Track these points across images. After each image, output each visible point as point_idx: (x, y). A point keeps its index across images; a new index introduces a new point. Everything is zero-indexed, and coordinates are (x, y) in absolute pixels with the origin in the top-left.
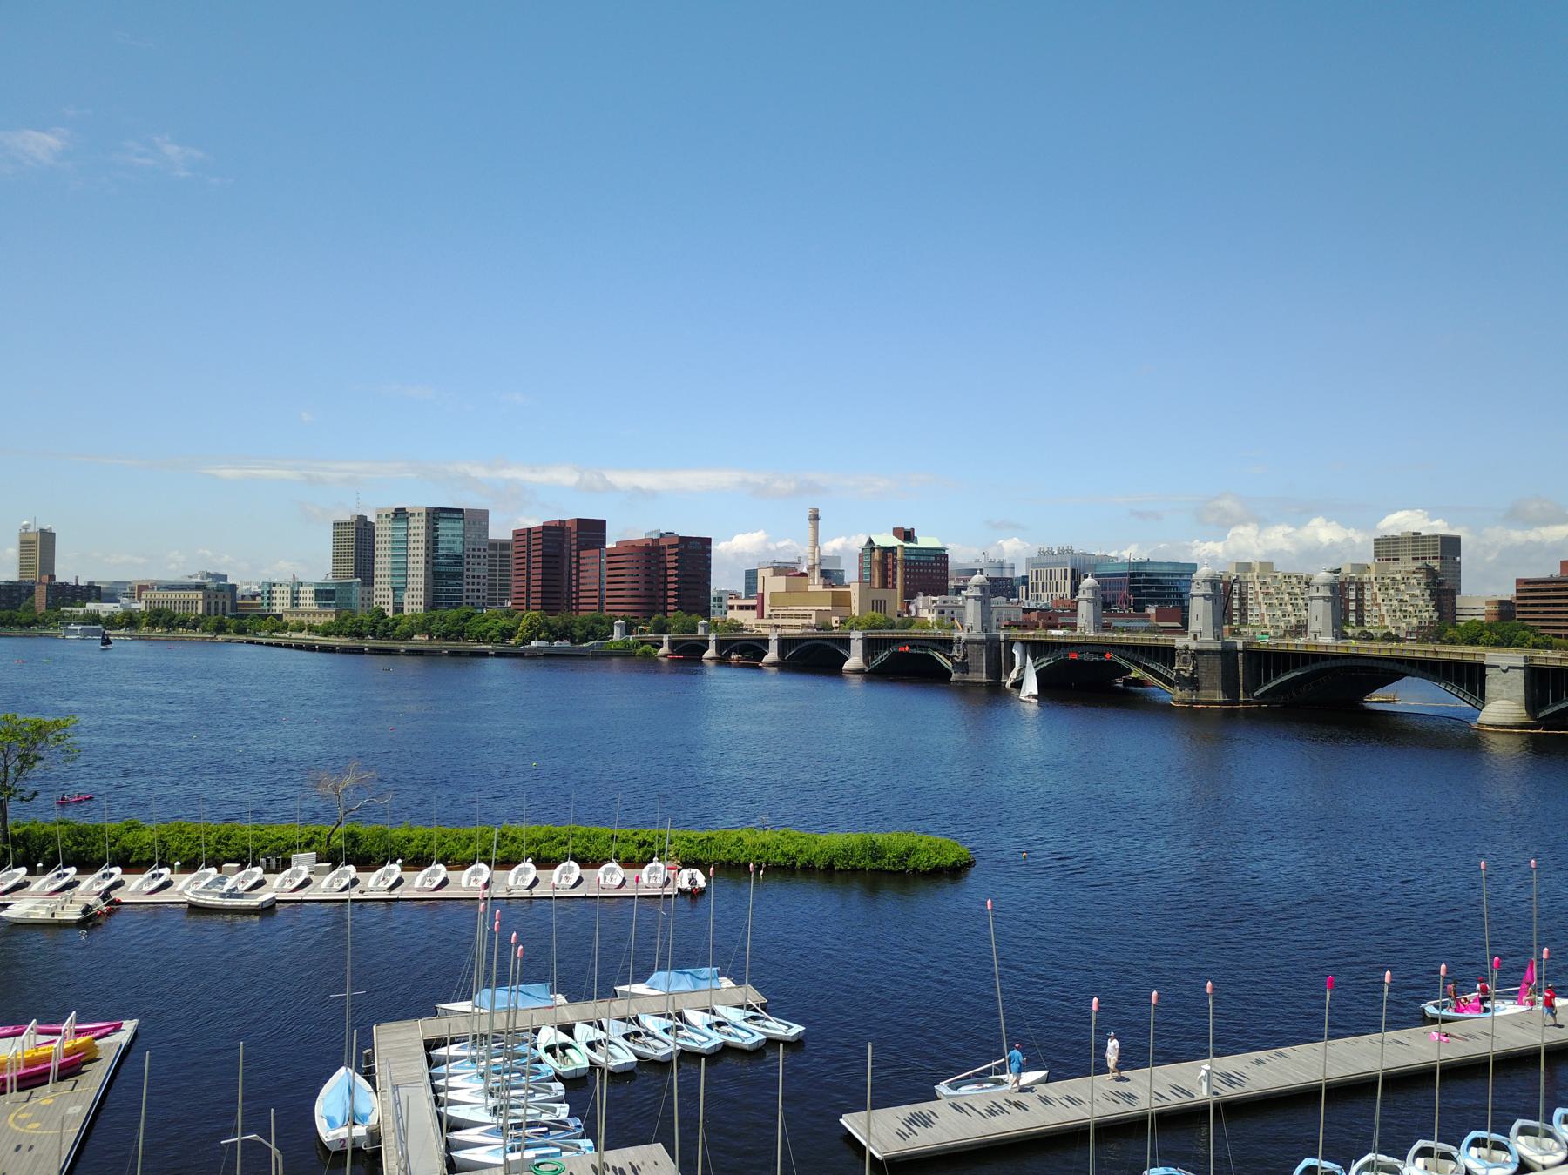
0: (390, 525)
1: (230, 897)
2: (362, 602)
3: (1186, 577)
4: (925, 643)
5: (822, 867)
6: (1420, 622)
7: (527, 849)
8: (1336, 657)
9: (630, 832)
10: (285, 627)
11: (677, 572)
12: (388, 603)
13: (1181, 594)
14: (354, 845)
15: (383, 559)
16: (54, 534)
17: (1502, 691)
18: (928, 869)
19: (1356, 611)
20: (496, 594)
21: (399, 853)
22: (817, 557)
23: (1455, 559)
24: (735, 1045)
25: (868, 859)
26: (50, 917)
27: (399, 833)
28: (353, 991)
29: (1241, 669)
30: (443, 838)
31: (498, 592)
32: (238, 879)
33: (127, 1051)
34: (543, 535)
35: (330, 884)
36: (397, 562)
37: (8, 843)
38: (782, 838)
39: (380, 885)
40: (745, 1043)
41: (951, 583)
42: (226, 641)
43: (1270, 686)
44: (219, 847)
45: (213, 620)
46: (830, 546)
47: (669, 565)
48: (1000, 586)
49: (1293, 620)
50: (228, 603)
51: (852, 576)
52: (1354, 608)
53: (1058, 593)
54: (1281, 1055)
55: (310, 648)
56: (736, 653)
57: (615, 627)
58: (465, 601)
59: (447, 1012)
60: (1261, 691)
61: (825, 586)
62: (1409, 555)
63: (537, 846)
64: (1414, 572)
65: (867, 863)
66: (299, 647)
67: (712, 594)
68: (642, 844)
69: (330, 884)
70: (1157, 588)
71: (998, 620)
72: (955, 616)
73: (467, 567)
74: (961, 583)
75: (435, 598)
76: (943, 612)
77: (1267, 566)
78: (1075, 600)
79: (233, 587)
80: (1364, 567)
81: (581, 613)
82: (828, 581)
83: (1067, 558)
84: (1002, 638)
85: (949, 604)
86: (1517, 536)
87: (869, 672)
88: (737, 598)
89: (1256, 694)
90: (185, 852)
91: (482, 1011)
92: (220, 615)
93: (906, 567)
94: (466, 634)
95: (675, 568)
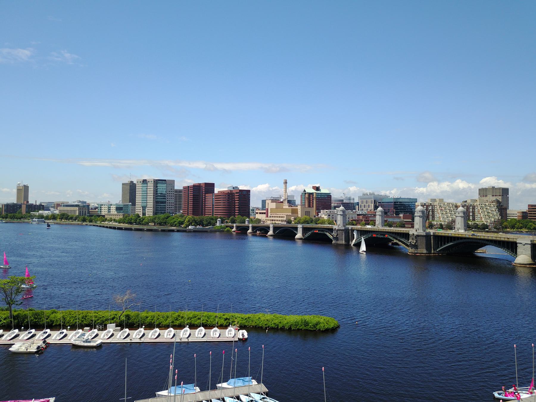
0: (141, 185)
1: (86, 342)
2: (132, 211)
3: (413, 203)
5: (287, 329)
6: (495, 220)
7: (187, 321)
8: (465, 238)
9: (222, 314)
10: (106, 220)
11: (238, 202)
12: (140, 212)
14: (128, 319)
15: (139, 197)
16: (28, 186)
17: (523, 252)
18: (324, 330)
19: (472, 216)
20: (177, 208)
21: (143, 322)
22: (286, 196)
23: (507, 196)
25: (303, 326)
26: (26, 351)
29: (432, 242)
31: (178, 207)
34: (193, 192)
36: (144, 198)
37: (12, 318)
38: (273, 317)
41: (333, 205)
43: (442, 248)
44: (83, 320)
45: (81, 217)
46: (291, 189)
47: (236, 199)
48: (349, 206)
49: (450, 219)
50: (87, 211)
51: (298, 201)
52: (471, 211)
55: (114, 228)
56: (259, 231)
58: (167, 211)
59: (159, 395)
61: (289, 206)
65: (303, 327)
66: (110, 228)
67: (250, 208)
68: (226, 319)
70: (403, 207)
71: (348, 218)
72: (334, 217)
75: (156, 210)
76: (330, 215)
78: (375, 211)
80: (475, 201)
82: (290, 205)
83: (372, 196)
84: (350, 229)
85: (332, 213)
86: (528, 186)
87: (304, 239)
88: (259, 210)
89: (437, 250)
93: (317, 200)
94: (167, 223)
95: (238, 200)
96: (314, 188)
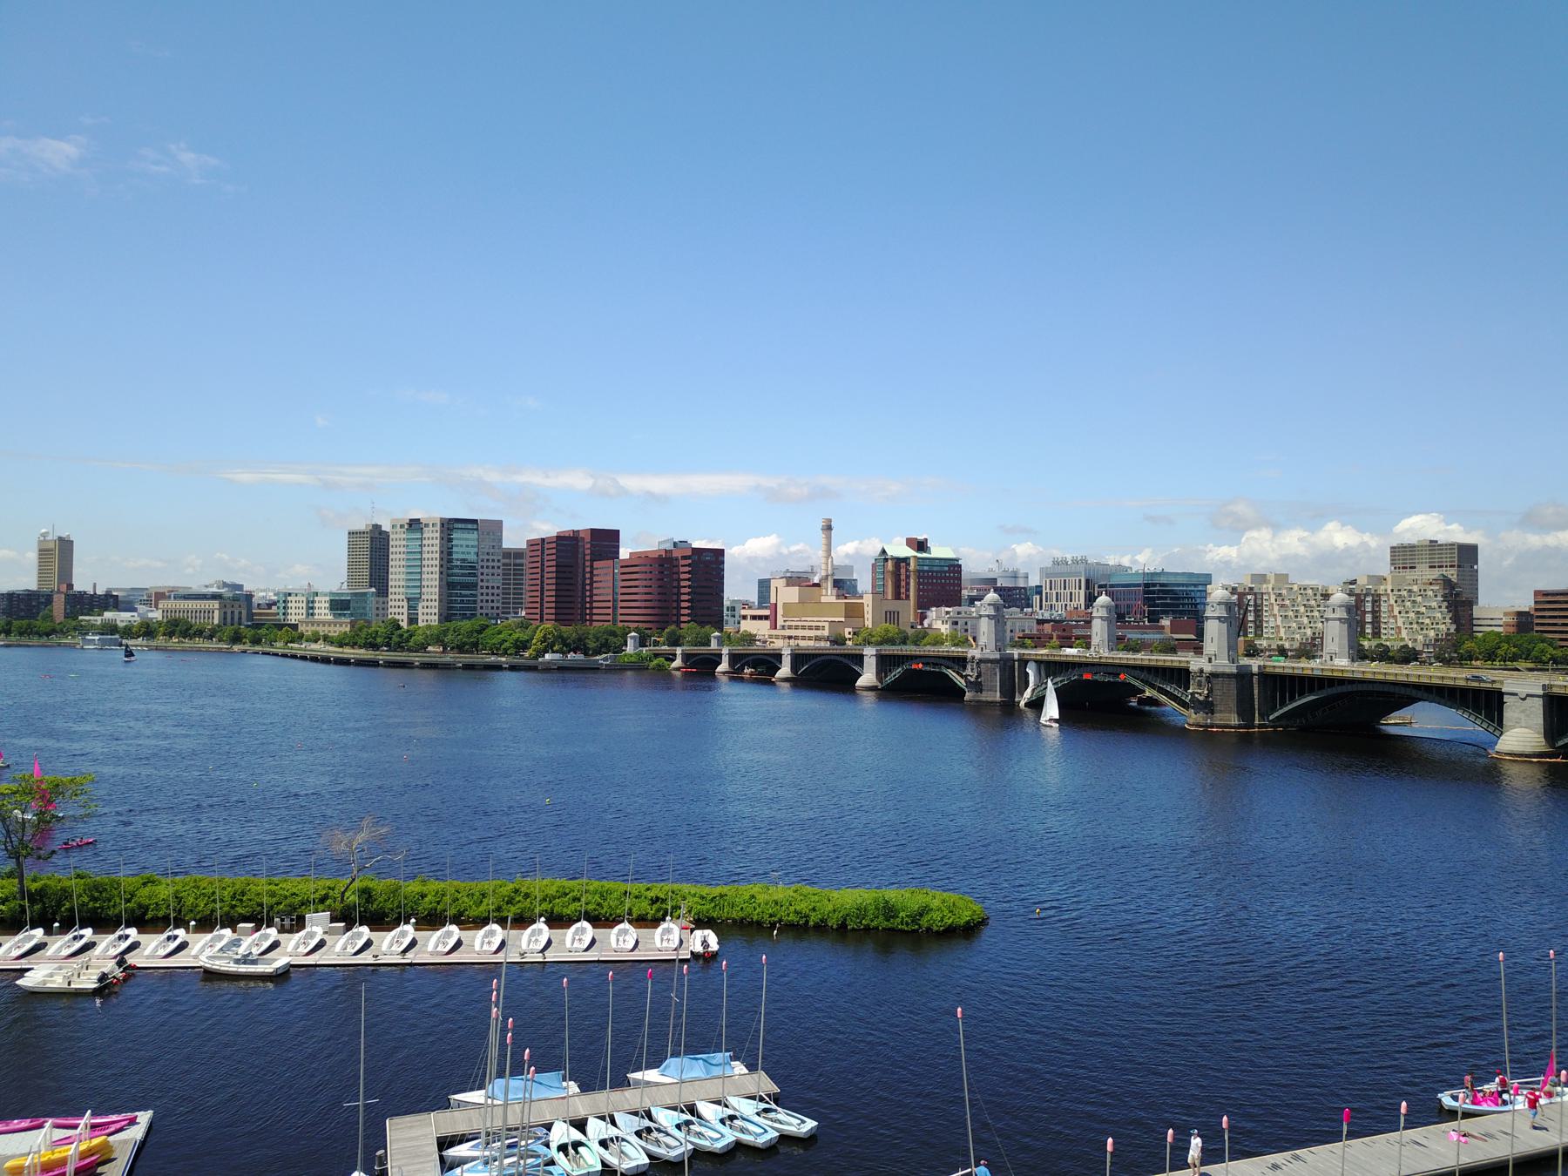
0: (404, 536)
1: (245, 963)
3: (1200, 588)
4: (942, 661)
5: (835, 927)
6: (1437, 635)
7: (540, 905)
8: (1352, 681)
11: (690, 583)
12: (403, 614)
13: (1196, 605)
15: (398, 570)
16: (72, 541)
17: (1520, 719)
18: (941, 928)
19: (1372, 623)
20: (511, 601)
21: (412, 909)
23: (1472, 567)
24: (745, 1143)
25: (881, 918)
26: (66, 986)
27: (413, 887)
28: (369, 1098)
29: (1256, 692)
30: (457, 894)
32: (252, 941)
33: (142, 1146)
35: (343, 947)
38: (794, 895)
39: (393, 948)
40: (758, 1141)
41: (965, 593)
42: (242, 652)
43: (1286, 709)
44: (234, 903)
45: (229, 630)
46: (845, 550)
47: (682, 576)
48: (1014, 596)
49: (1309, 632)
50: (244, 612)
51: (864, 583)
52: (1370, 610)
53: (1072, 603)
54: (1297, 1158)
55: (326, 660)
56: (749, 667)
57: (629, 640)
58: (479, 611)
59: (460, 1104)
60: (1276, 714)
61: (838, 597)
62: (1426, 563)
63: (550, 902)
64: (1431, 584)
65: (881, 923)
66: (314, 659)
67: (725, 603)
68: (655, 900)
69: (343, 947)
70: (1171, 599)
71: (1011, 631)
73: (481, 577)
74: (975, 593)
75: (450, 608)
76: (956, 623)
77: (1282, 578)
79: (249, 597)
81: (595, 624)
82: (841, 592)
83: (1081, 568)
84: (1016, 657)
85: (963, 615)
86: (1534, 540)
87: (882, 689)
88: (750, 608)
89: (1271, 718)
90: (200, 909)
91: (496, 1102)
92: (236, 626)
93: (919, 578)
94: (480, 647)
95: (688, 580)
96: (910, 542)
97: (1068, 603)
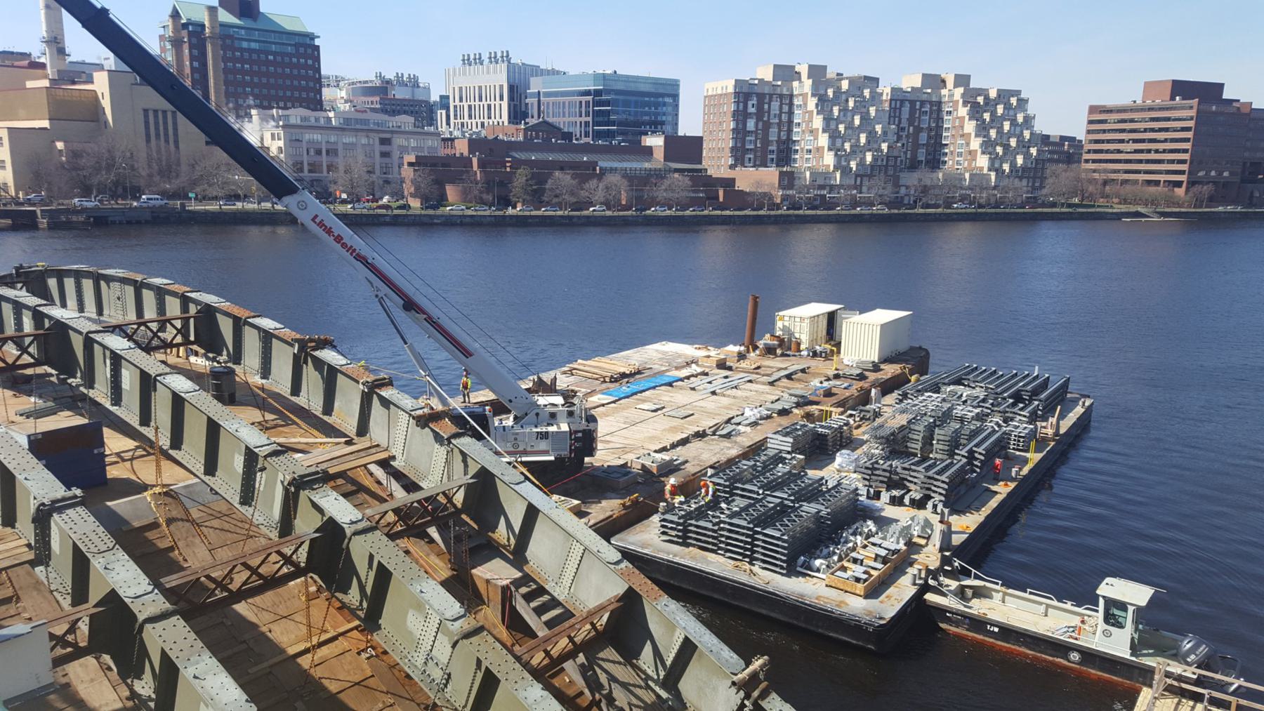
97: (486, 121)
